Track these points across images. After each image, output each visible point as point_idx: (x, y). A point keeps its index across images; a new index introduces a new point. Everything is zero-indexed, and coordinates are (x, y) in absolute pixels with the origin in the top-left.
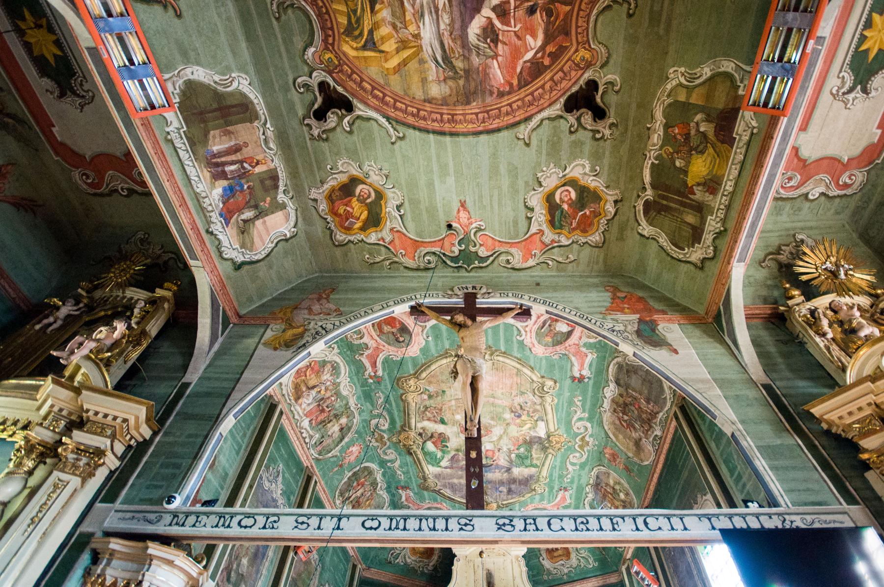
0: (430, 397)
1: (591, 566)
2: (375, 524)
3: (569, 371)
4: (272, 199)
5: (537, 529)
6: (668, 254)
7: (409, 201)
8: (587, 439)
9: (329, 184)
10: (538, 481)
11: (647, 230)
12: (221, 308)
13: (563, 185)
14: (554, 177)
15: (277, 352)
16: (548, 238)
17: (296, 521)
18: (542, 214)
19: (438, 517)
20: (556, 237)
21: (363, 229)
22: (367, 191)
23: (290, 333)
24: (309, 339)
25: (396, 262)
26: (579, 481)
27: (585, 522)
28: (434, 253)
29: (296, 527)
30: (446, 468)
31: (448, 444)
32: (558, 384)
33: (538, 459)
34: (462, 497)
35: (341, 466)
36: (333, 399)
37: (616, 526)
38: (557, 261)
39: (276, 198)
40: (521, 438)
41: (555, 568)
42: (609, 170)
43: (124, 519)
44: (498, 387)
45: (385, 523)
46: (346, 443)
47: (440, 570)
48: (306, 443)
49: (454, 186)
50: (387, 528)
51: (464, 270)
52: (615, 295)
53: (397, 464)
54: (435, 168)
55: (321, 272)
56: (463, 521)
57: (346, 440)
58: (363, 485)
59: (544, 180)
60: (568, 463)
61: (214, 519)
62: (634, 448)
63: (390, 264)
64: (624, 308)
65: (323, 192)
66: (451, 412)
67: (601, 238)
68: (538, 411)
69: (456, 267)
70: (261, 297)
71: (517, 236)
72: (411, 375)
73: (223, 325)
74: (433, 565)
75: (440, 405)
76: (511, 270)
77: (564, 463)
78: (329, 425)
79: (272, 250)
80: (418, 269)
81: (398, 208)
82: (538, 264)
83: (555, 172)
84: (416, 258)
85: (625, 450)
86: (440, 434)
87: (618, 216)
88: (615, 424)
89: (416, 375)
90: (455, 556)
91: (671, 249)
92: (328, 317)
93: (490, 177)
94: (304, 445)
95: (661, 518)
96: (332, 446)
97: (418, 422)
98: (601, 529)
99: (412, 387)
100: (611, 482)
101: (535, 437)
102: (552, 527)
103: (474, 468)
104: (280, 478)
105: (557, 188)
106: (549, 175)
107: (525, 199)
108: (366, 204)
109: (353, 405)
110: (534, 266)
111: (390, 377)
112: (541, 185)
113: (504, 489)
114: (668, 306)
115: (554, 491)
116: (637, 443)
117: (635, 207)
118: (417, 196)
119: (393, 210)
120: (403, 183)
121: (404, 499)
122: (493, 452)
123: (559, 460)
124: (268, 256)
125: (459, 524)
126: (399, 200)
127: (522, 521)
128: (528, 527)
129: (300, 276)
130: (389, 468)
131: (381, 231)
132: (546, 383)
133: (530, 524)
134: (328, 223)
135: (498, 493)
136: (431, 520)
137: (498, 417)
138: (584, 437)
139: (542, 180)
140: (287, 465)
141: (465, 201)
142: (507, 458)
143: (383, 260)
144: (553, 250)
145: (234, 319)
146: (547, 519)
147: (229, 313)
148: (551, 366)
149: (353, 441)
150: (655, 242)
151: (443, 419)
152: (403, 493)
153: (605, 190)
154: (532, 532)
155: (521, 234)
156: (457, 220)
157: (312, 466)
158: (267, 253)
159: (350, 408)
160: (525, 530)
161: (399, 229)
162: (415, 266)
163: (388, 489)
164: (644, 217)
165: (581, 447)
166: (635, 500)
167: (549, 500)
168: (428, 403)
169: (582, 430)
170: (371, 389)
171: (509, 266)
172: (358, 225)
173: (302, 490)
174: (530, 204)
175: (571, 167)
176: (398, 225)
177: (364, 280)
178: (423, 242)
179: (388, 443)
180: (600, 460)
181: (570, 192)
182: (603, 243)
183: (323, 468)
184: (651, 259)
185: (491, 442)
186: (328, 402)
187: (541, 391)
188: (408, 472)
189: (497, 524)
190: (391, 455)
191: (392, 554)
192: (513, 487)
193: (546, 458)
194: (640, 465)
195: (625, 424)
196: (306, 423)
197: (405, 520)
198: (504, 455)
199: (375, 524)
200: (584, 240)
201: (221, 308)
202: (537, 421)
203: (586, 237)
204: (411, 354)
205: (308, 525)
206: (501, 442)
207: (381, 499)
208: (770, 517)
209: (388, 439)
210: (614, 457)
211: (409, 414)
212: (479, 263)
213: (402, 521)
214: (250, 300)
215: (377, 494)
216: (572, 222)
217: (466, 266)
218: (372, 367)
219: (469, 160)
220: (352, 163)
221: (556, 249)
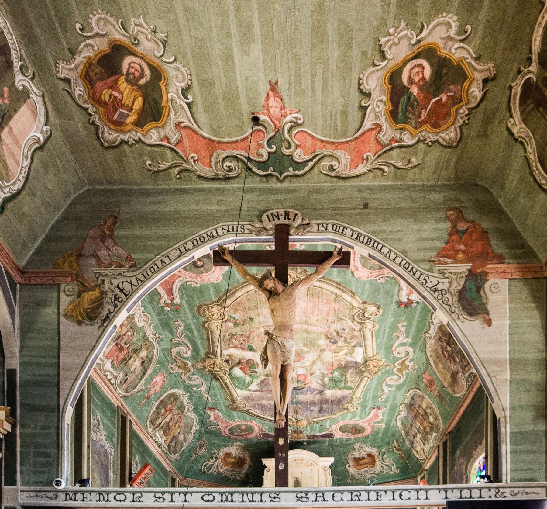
0: (236, 324)
1: (393, 473)
2: (211, 498)
3: (395, 296)
4: (9, 88)
5: (324, 500)
6: (531, 173)
7: (198, 81)
8: (407, 363)
9: (83, 55)
10: (351, 401)
11: (518, 127)
12: (3, 269)
13: (415, 57)
14: (405, 42)
15: (83, 328)
16: (387, 136)
17: (155, 496)
18: (381, 101)
19: (255, 492)
20: (397, 135)
21: (139, 124)
22: (138, 67)
23: (88, 297)
24: (110, 307)
25: (187, 170)
26: (394, 400)
27: (359, 494)
28: (236, 158)
29: (156, 501)
30: (255, 391)
31: (257, 370)
32: (381, 310)
33: (352, 382)
34: (272, 416)
35: (148, 398)
36: (130, 334)
37: (379, 498)
38: (394, 166)
39: (13, 84)
40: (336, 363)
41: (359, 474)
42: (484, 31)
43: (30, 497)
44: (313, 314)
45: (218, 497)
46: (149, 376)
47: (251, 477)
48: (112, 385)
49: (261, 59)
50: (220, 500)
51: (275, 180)
52: (454, 226)
53: (204, 388)
54: (234, 30)
55: (91, 183)
56: (273, 495)
57: (149, 372)
58: (171, 410)
59: (390, 48)
60: (384, 385)
61: (95, 496)
62: (450, 379)
63: (180, 172)
64: (458, 251)
65: (76, 67)
66: (259, 339)
67: (457, 135)
68: (357, 337)
69: (265, 176)
70: (34, 238)
71: (345, 133)
72: (213, 302)
73: (12, 292)
74: (245, 473)
75: (248, 333)
76: (335, 180)
77: (380, 385)
78: (130, 362)
79: (29, 169)
80: (215, 179)
81: (185, 92)
82: (370, 171)
83: (407, 36)
84: (213, 164)
85: (442, 379)
86: (249, 360)
87: (484, 103)
88: (437, 352)
89: (220, 302)
90: (265, 467)
91: (536, 167)
92: (121, 270)
93: (313, 45)
94: (111, 387)
95: (412, 492)
96: (137, 381)
97: (224, 349)
98: (369, 500)
99: (215, 315)
100: (424, 406)
101: (351, 362)
102: (335, 499)
103: (282, 453)
104: (101, 426)
105: (406, 62)
106: (396, 40)
107: (360, 79)
108: (140, 87)
109: (151, 335)
110: (365, 174)
111: (189, 305)
112: (383, 57)
113: (316, 409)
114: (511, 247)
115: (367, 409)
116: (454, 376)
117: (511, 88)
118: (210, 75)
119: (178, 95)
120: (189, 53)
121: (212, 418)
122: (306, 376)
123: (375, 381)
124: (26, 181)
125: (270, 497)
126: (184, 80)
127: (315, 494)
128: (318, 499)
129: (68, 195)
130: (196, 392)
131: (163, 126)
132: (368, 309)
133: (320, 497)
134: (91, 115)
135: (309, 412)
136: (250, 495)
137: (312, 344)
138: (404, 361)
139: (386, 49)
140: (103, 412)
141: (276, 83)
142: (320, 382)
143: (170, 167)
144: (392, 153)
145: (18, 279)
146: (332, 493)
147: (12, 273)
148: (375, 290)
149: (156, 371)
150: (522, 149)
151: (251, 346)
152: (212, 414)
153: (473, 63)
154: (320, 502)
155: (351, 131)
156: (266, 111)
157: (122, 405)
158: (25, 175)
159: (148, 339)
160: (316, 500)
161: (188, 124)
162: (211, 175)
163: (196, 410)
164: (520, 105)
165: (400, 370)
166: (442, 425)
167: (361, 417)
168: (234, 331)
169: (403, 355)
170: (168, 317)
171: (333, 174)
172: (132, 118)
173: (120, 430)
174: (366, 87)
175: (431, 26)
176: (185, 118)
177: (149, 200)
178: (219, 142)
179: (192, 370)
180: (417, 383)
181: (423, 68)
182: (459, 142)
183: (132, 403)
184: (512, 172)
185: (304, 367)
186: (126, 338)
187: (362, 317)
188: (215, 395)
189: (297, 497)
190: (197, 380)
191: (205, 466)
192: (325, 406)
193: (360, 382)
194: (452, 396)
195: (446, 355)
196: (108, 366)
197: (232, 495)
198: (317, 378)
199: (211, 498)
200: (433, 138)
201: (3, 269)
202: (354, 346)
203: (437, 133)
204: (212, 280)
205: (164, 499)
206: (315, 366)
207: (189, 420)
208: (490, 490)
209: (193, 366)
210: (431, 383)
211: (213, 342)
212: (294, 170)
213: (230, 496)
214: (25, 247)
215: (185, 416)
216: (420, 113)
217: (277, 174)
218: (168, 295)
219: (282, 17)
220: (110, 18)
221: (396, 151)
